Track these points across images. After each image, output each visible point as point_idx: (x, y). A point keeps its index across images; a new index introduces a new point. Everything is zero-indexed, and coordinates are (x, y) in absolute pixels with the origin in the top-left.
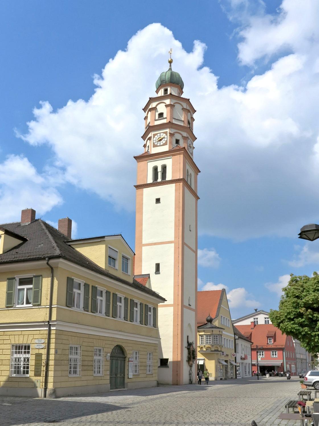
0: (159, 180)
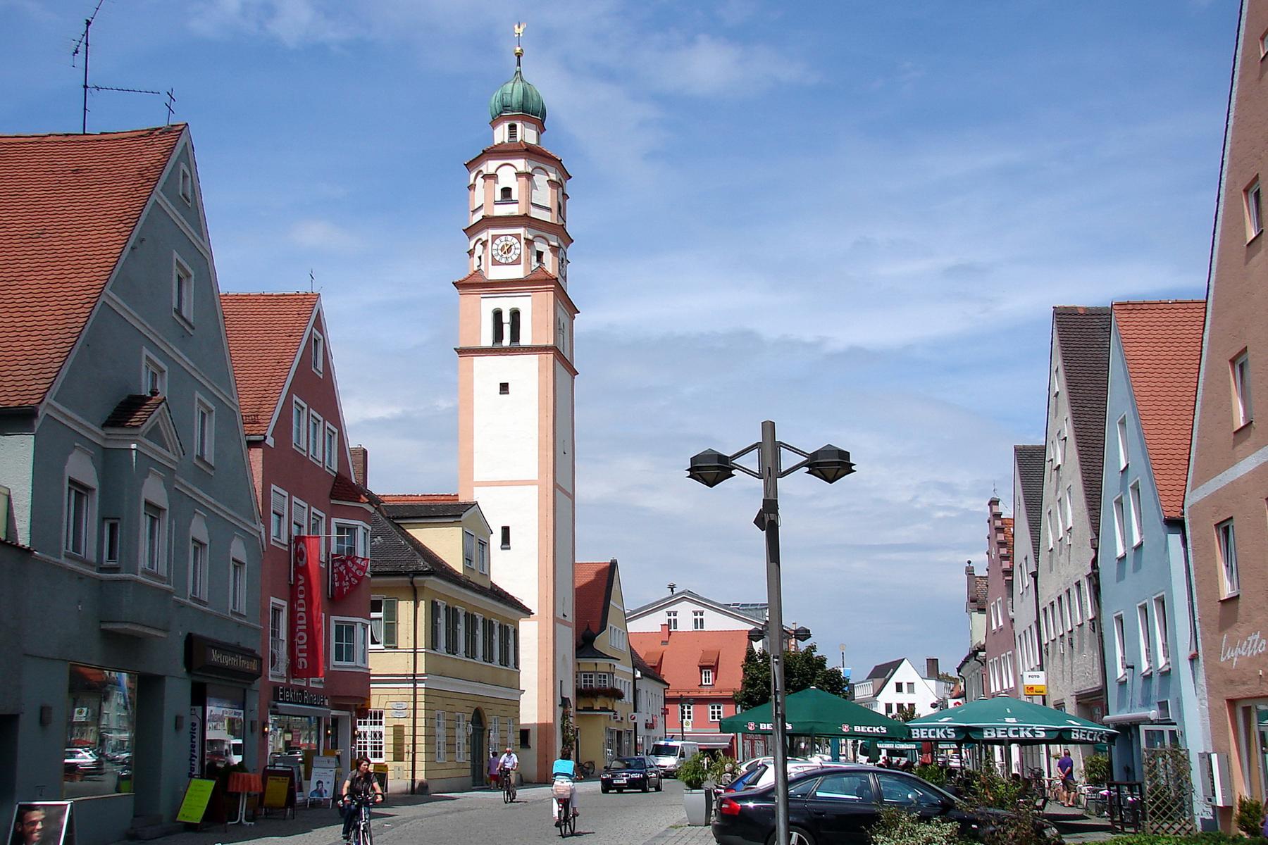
0: (506, 342)
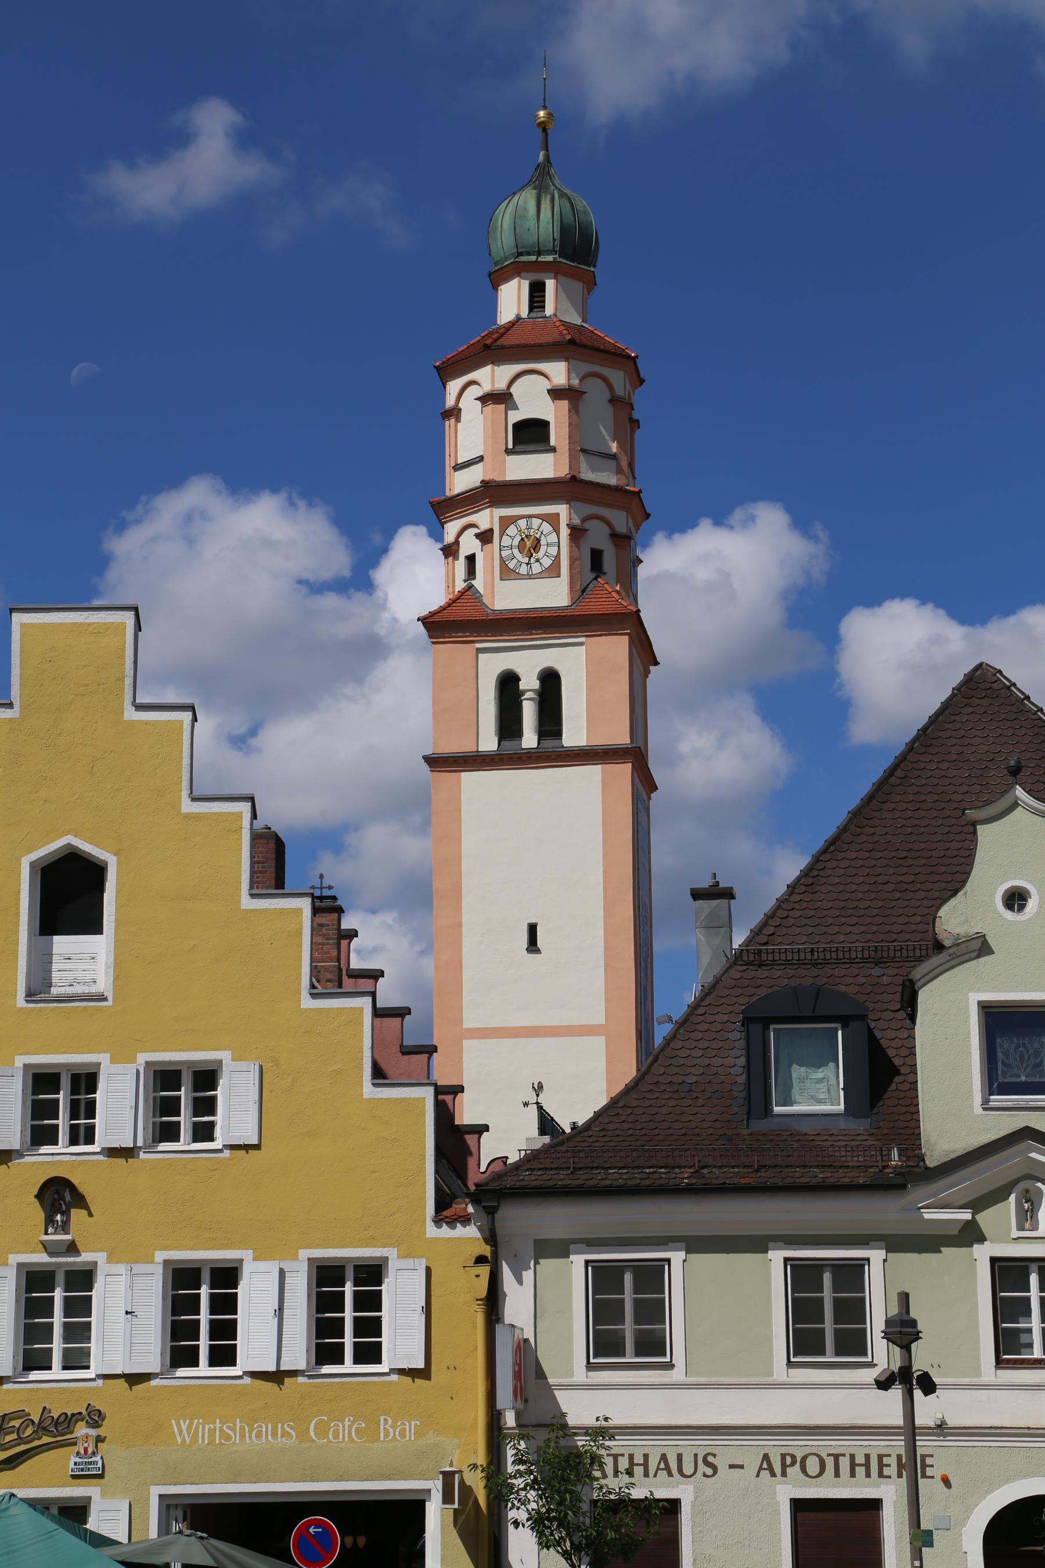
0: (529, 739)
